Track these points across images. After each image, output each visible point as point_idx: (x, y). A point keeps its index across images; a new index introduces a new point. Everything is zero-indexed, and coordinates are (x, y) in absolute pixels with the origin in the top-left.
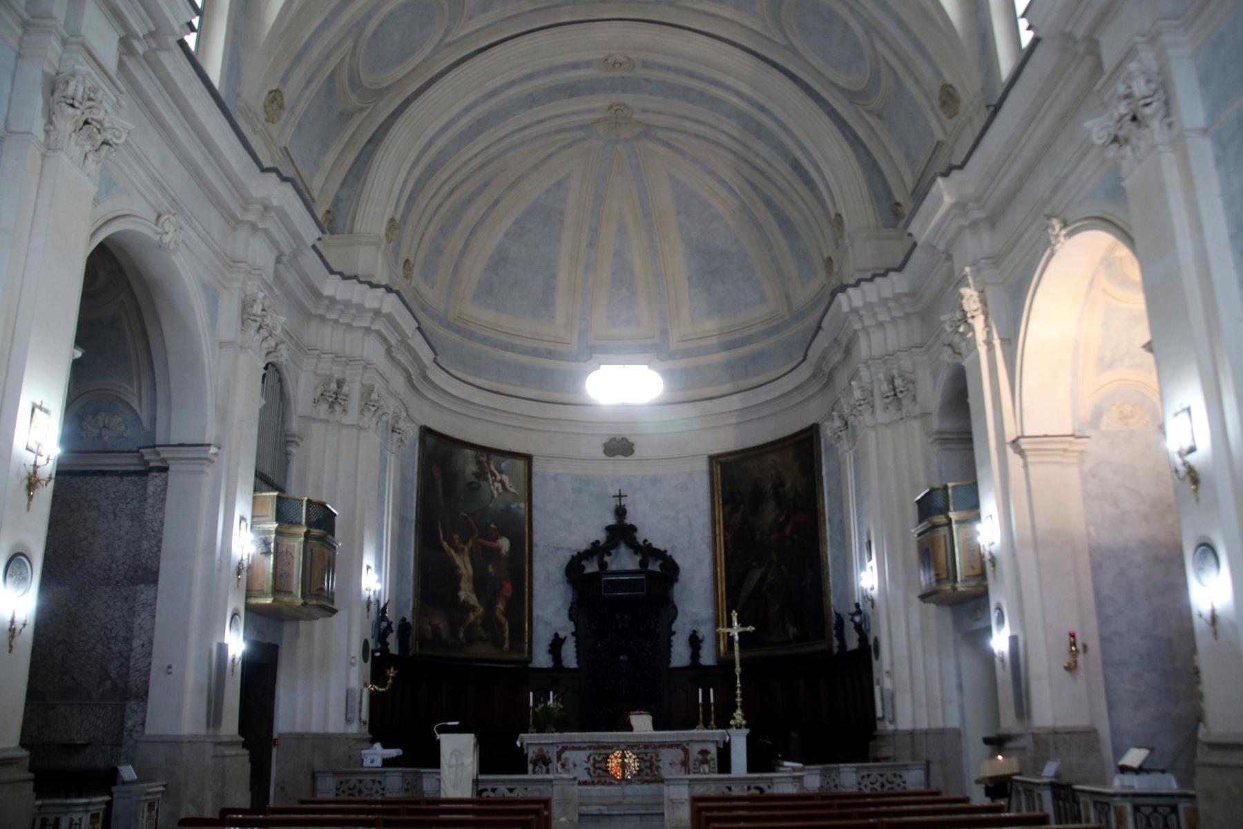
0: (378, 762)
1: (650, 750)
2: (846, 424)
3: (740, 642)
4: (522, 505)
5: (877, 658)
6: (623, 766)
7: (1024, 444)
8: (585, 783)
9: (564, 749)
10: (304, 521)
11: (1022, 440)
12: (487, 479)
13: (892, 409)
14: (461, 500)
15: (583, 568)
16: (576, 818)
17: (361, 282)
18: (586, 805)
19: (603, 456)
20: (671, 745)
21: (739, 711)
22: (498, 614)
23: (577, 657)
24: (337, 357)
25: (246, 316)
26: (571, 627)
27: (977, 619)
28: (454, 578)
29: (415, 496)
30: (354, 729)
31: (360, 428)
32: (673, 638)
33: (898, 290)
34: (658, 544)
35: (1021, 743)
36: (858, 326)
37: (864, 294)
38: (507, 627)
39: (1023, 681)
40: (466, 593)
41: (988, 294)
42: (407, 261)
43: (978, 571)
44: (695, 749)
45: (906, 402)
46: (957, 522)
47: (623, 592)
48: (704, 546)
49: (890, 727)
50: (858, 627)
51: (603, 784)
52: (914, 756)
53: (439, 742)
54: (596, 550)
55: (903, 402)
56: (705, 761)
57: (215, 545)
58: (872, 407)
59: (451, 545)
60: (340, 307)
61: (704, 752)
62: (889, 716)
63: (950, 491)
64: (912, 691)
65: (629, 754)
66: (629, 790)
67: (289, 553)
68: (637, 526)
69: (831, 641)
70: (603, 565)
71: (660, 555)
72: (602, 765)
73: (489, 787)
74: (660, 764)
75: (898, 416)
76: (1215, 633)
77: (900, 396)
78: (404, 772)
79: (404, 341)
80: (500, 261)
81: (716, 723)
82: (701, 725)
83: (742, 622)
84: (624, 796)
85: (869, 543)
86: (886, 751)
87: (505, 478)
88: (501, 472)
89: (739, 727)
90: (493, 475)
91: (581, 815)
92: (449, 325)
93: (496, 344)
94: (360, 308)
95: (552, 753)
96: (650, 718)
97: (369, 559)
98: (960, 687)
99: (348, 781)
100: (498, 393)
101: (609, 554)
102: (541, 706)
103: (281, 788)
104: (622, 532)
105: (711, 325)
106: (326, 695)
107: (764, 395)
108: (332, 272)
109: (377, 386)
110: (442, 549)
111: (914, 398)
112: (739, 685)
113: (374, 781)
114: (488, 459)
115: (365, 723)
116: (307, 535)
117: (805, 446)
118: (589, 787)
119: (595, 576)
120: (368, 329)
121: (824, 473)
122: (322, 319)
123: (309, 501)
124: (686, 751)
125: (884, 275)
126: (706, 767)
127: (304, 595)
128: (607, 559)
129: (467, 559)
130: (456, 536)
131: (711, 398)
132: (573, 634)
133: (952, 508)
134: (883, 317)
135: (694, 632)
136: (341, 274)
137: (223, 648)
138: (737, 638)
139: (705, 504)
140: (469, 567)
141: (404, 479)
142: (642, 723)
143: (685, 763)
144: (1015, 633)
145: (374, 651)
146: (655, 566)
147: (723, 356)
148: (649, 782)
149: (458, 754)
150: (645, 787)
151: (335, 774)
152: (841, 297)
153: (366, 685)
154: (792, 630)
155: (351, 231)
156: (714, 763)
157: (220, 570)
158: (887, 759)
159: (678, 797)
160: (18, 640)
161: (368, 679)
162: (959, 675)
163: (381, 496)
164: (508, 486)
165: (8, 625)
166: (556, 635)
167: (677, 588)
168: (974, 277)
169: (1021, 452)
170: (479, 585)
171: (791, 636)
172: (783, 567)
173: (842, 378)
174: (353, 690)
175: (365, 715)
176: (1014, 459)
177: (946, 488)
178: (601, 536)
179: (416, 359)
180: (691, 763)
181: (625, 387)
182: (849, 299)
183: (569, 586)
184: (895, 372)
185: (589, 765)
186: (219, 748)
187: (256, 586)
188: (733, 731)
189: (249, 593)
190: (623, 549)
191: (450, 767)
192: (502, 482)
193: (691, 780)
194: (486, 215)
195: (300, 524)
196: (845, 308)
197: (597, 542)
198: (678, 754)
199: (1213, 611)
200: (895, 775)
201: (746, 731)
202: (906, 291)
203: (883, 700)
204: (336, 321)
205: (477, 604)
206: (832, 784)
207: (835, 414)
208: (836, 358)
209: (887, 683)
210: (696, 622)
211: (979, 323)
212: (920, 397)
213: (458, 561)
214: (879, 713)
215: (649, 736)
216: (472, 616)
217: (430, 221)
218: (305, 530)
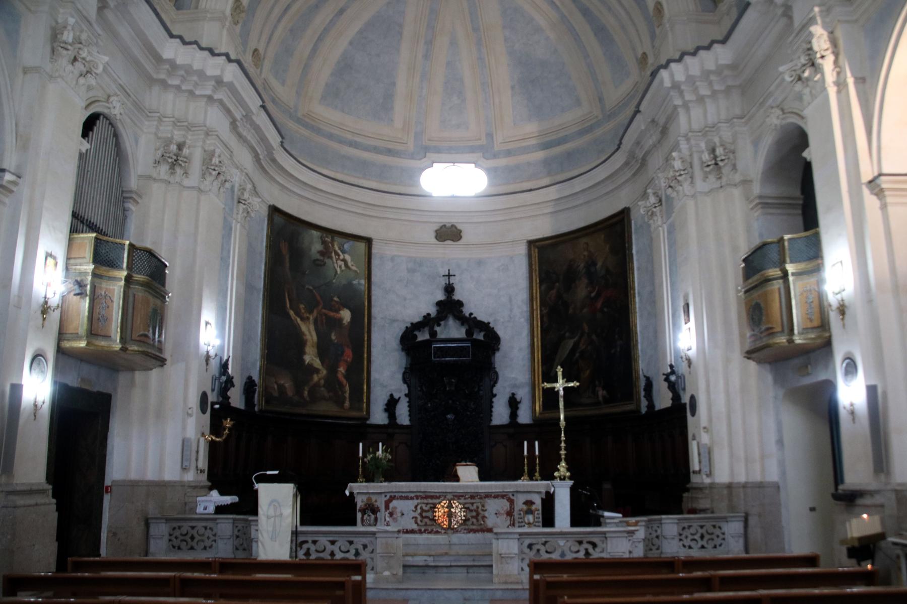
0: (211, 509)
1: (477, 500)
2: (660, 201)
4: (363, 282)
5: (693, 414)
6: (450, 515)
7: (884, 183)
8: (412, 532)
9: (392, 498)
10: (125, 265)
11: (882, 178)
12: (331, 257)
13: (712, 178)
14: (302, 274)
15: (416, 337)
16: (400, 571)
17: (201, 49)
18: (413, 556)
19: (434, 240)
20: (496, 496)
21: (563, 464)
22: (340, 376)
23: (410, 415)
24: (177, 123)
25: (55, 45)
26: (405, 389)
27: (808, 374)
28: (300, 344)
30: (190, 476)
31: (200, 190)
32: (494, 400)
33: (722, 62)
34: (482, 317)
35: (878, 499)
36: (678, 102)
37: (687, 69)
38: (347, 388)
39: (882, 433)
40: (311, 357)
41: (839, 33)
42: (256, 50)
43: (816, 323)
44: (520, 500)
45: (725, 171)
46: (793, 274)
47: (450, 357)
48: (522, 320)
49: (707, 481)
50: (672, 386)
52: (732, 508)
53: (257, 491)
54: (427, 322)
55: (724, 171)
56: (529, 512)
57: (10, 279)
58: (692, 177)
59: (298, 314)
60: (182, 72)
62: (705, 470)
63: (786, 244)
64: (731, 447)
65: (455, 503)
66: (455, 538)
67: (108, 298)
68: (464, 302)
69: (639, 401)
70: (433, 334)
71: (485, 327)
72: (429, 514)
73: (310, 539)
74: (486, 514)
75: (718, 184)
76: (854, 419)
77: (721, 164)
78: (234, 520)
79: (248, 117)
80: (345, 67)
81: (540, 475)
82: (526, 477)
83: (568, 377)
84: (450, 545)
85: (687, 305)
86: (703, 504)
87: (348, 257)
88: (344, 252)
89: (563, 479)
90: (337, 254)
91: (405, 566)
92: (299, 121)
93: (341, 141)
94: (201, 74)
95: (380, 503)
96: (476, 469)
97: (208, 314)
98: (780, 442)
99: (180, 528)
100: (342, 182)
101: (439, 325)
102: (369, 457)
103: (113, 534)
104: (450, 306)
105: (531, 128)
106: (158, 444)
107: (578, 185)
108: (172, 36)
109: (218, 151)
111: (734, 167)
112: (563, 438)
113: (206, 528)
114: (333, 240)
115: (202, 471)
116: (128, 279)
117: (616, 230)
119: (427, 343)
120: (210, 98)
121: (634, 251)
122: (164, 84)
123: (131, 246)
124: (512, 502)
125: (708, 48)
126: (530, 518)
127: (122, 339)
128: (437, 329)
129: (312, 327)
130: (302, 306)
131: (531, 190)
132: (406, 395)
133: (788, 260)
134: (704, 91)
135: (513, 394)
136: (180, 38)
137: (17, 389)
138: (562, 393)
139: (523, 283)
140: (314, 334)
141: (251, 250)
142: (468, 474)
143: (510, 513)
144: (873, 383)
145: (213, 404)
146: (480, 336)
147: (540, 155)
148: (475, 531)
149: (277, 501)
150: (471, 535)
151: (168, 520)
152: (664, 73)
153: (203, 435)
154: (601, 393)
155: (197, 8)
156: (539, 514)
157: (18, 307)
158: (704, 511)
159: (511, 564)
160: (39, 412)
161: (207, 430)
162: (779, 430)
163: (224, 260)
164: (350, 264)
165: (33, 402)
166: (391, 395)
167: (498, 356)
168: (823, 17)
169: (879, 193)
170: (323, 350)
171: (601, 399)
172: (594, 337)
173: (656, 161)
174: (189, 440)
175: (203, 463)
176: (871, 201)
177: (781, 240)
178: (433, 311)
179: (263, 139)
180: (516, 513)
181: (453, 182)
182: (672, 75)
183: (403, 353)
184: (716, 140)
186: (11, 497)
187: (70, 329)
188: (557, 482)
189: (61, 335)
190: (451, 322)
191: (268, 517)
192: (344, 260)
193: (521, 534)
194: (332, 23)
195: (122, 268)
196: (667, 83)
197: (429, 315)
198: (504, 504)
199: (852, 405)
200: (714, 526)
201: (571, 483)
202: (730, 63)
203: (699, 454)
204: (178, 88)
206: (654, 535)
207: (649, 191)
208: (649, 142)
209: (705, 439)
210: (515, 386)
211: (828, 65)
212: (740, 166)
213: (304, 328)
214: (695, 465)
215: (476, 487)
216: (316, 378)
217: (279, 21)
218: (125, 273)
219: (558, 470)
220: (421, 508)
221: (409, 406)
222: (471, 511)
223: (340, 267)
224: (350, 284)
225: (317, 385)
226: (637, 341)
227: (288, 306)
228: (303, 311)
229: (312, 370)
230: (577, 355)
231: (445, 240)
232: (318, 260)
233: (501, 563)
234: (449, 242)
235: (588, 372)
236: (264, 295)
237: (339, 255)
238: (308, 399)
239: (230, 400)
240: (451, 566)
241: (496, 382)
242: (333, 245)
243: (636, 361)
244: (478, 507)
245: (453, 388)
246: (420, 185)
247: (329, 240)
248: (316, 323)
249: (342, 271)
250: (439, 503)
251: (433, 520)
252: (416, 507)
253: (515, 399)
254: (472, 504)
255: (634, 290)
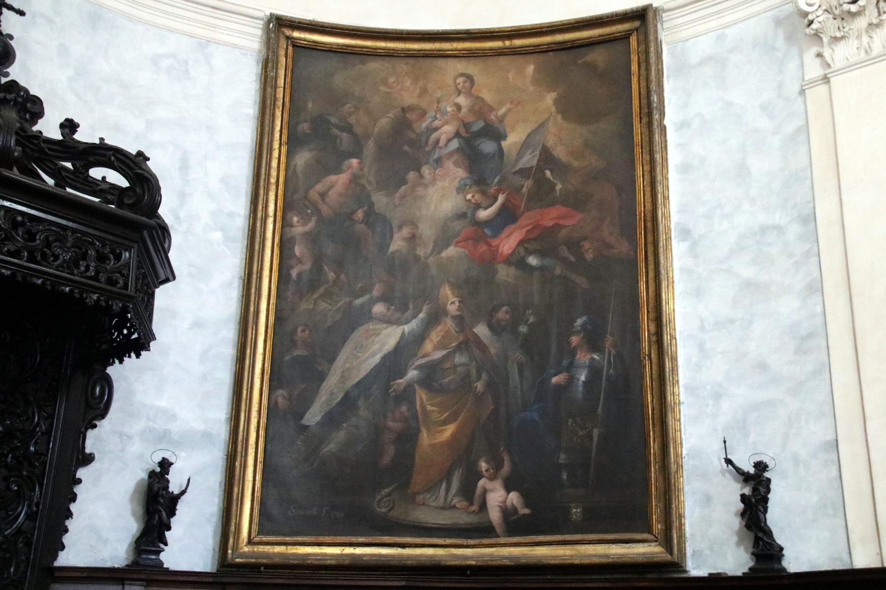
100: (203, 5)
154: (498, 498)
171: (495, 515)
172: (482, 330)
230: (412, 374)
235: (449, 430)
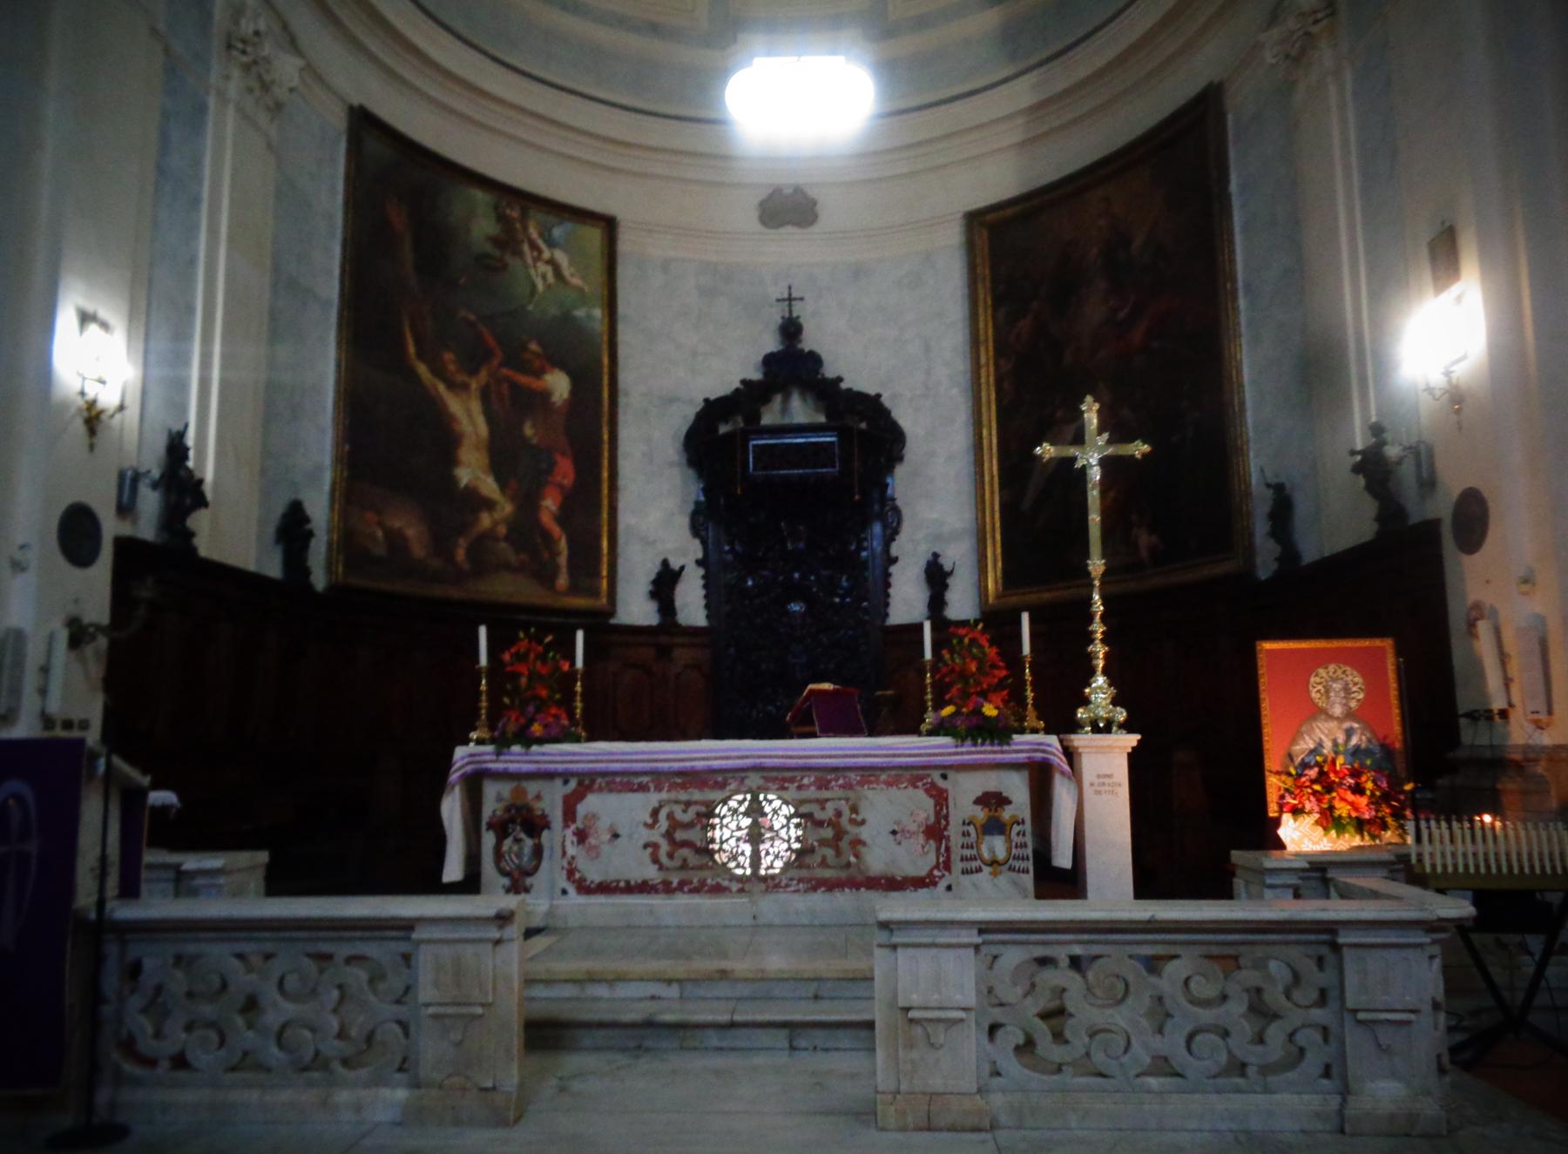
3: (1105, 485)
4: (598, 313)
8: (644, 888)
12: (518, 253)
19: (758, 227)
21: (1100, 680)
22: (546, 519)
23: (707, 606)
26: (695, 549)
28: (446, 442)
29: (337, 250)
32: (893, 569)
38: (563, 544)
40: (472, 470)
44: (965, 791)
47: (789, 467)
48: (955, 391)
51: (696, 891)
54: (748, 399)
56: (995, 826)
59: (439, 372)
61: (993, 800)
68: (824, 356)
69: (1251, 548)
72: (693, 835)
74: (864, 833)
83: (1116, 428)
87: (561, 257)
90: (534, 246)
95: (550, 800)
104: (792, 365)
107: (1085, 63)
110: (412, 374)
114: (524, 217)
118: (657, 901)
121: (1234, 187)
124: (940, 798)
126: (997, 846)
129: (476, 407)
132: (699, 563)
135: (936, 555)
138: (1096, 474)
143: (935, 832)
148: (831, 886)
150: (819, 899)
166: (665, 563)
167: (900, 471)
171: (1144, 553)
180: (954, 832)
183: (691, 473)
185: (656, 836)
192: (552, 262)
193: (984, 928)
201: (1133, 739)
205: (489, 486)
210: (938, 538)
213: (454, 405)
216: (486, 520)
219: (1085, 702)
220: (670, 816)
221: (705, 586)
222: (820, 824)
223: (544, 277)
224: (566, 319)
225: (489, 535)
226: (1242, 404)
227: (412, 349)
228: (452, 367)
229: (475, 501)
231: (780, 225)
232: (486, 256)
233: (910, 1045)
234: (790, 229)
236: (341, 316)
237: (540, 252)
238: (466, 566)
239: (197, 541)
240: (733, 1025)
241: (896, 532)
242: (525, 229)
243: (1241, 451)
244: (839, 814)
245: (801, 545)
246: (720, 100)
247: (515, 214)
248: (485, 396)
249: (548, 287)
250: (725, 802)
251: (706, 851)
252: (655, 813)
253: (941, 567)
254: (822, 803)
255: (1234, 281)
